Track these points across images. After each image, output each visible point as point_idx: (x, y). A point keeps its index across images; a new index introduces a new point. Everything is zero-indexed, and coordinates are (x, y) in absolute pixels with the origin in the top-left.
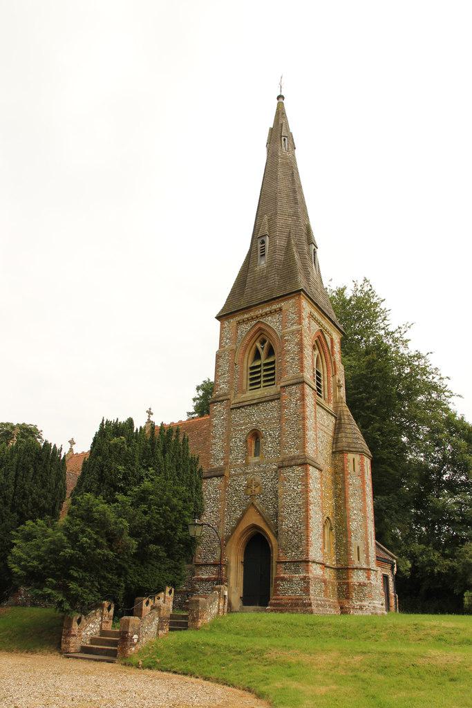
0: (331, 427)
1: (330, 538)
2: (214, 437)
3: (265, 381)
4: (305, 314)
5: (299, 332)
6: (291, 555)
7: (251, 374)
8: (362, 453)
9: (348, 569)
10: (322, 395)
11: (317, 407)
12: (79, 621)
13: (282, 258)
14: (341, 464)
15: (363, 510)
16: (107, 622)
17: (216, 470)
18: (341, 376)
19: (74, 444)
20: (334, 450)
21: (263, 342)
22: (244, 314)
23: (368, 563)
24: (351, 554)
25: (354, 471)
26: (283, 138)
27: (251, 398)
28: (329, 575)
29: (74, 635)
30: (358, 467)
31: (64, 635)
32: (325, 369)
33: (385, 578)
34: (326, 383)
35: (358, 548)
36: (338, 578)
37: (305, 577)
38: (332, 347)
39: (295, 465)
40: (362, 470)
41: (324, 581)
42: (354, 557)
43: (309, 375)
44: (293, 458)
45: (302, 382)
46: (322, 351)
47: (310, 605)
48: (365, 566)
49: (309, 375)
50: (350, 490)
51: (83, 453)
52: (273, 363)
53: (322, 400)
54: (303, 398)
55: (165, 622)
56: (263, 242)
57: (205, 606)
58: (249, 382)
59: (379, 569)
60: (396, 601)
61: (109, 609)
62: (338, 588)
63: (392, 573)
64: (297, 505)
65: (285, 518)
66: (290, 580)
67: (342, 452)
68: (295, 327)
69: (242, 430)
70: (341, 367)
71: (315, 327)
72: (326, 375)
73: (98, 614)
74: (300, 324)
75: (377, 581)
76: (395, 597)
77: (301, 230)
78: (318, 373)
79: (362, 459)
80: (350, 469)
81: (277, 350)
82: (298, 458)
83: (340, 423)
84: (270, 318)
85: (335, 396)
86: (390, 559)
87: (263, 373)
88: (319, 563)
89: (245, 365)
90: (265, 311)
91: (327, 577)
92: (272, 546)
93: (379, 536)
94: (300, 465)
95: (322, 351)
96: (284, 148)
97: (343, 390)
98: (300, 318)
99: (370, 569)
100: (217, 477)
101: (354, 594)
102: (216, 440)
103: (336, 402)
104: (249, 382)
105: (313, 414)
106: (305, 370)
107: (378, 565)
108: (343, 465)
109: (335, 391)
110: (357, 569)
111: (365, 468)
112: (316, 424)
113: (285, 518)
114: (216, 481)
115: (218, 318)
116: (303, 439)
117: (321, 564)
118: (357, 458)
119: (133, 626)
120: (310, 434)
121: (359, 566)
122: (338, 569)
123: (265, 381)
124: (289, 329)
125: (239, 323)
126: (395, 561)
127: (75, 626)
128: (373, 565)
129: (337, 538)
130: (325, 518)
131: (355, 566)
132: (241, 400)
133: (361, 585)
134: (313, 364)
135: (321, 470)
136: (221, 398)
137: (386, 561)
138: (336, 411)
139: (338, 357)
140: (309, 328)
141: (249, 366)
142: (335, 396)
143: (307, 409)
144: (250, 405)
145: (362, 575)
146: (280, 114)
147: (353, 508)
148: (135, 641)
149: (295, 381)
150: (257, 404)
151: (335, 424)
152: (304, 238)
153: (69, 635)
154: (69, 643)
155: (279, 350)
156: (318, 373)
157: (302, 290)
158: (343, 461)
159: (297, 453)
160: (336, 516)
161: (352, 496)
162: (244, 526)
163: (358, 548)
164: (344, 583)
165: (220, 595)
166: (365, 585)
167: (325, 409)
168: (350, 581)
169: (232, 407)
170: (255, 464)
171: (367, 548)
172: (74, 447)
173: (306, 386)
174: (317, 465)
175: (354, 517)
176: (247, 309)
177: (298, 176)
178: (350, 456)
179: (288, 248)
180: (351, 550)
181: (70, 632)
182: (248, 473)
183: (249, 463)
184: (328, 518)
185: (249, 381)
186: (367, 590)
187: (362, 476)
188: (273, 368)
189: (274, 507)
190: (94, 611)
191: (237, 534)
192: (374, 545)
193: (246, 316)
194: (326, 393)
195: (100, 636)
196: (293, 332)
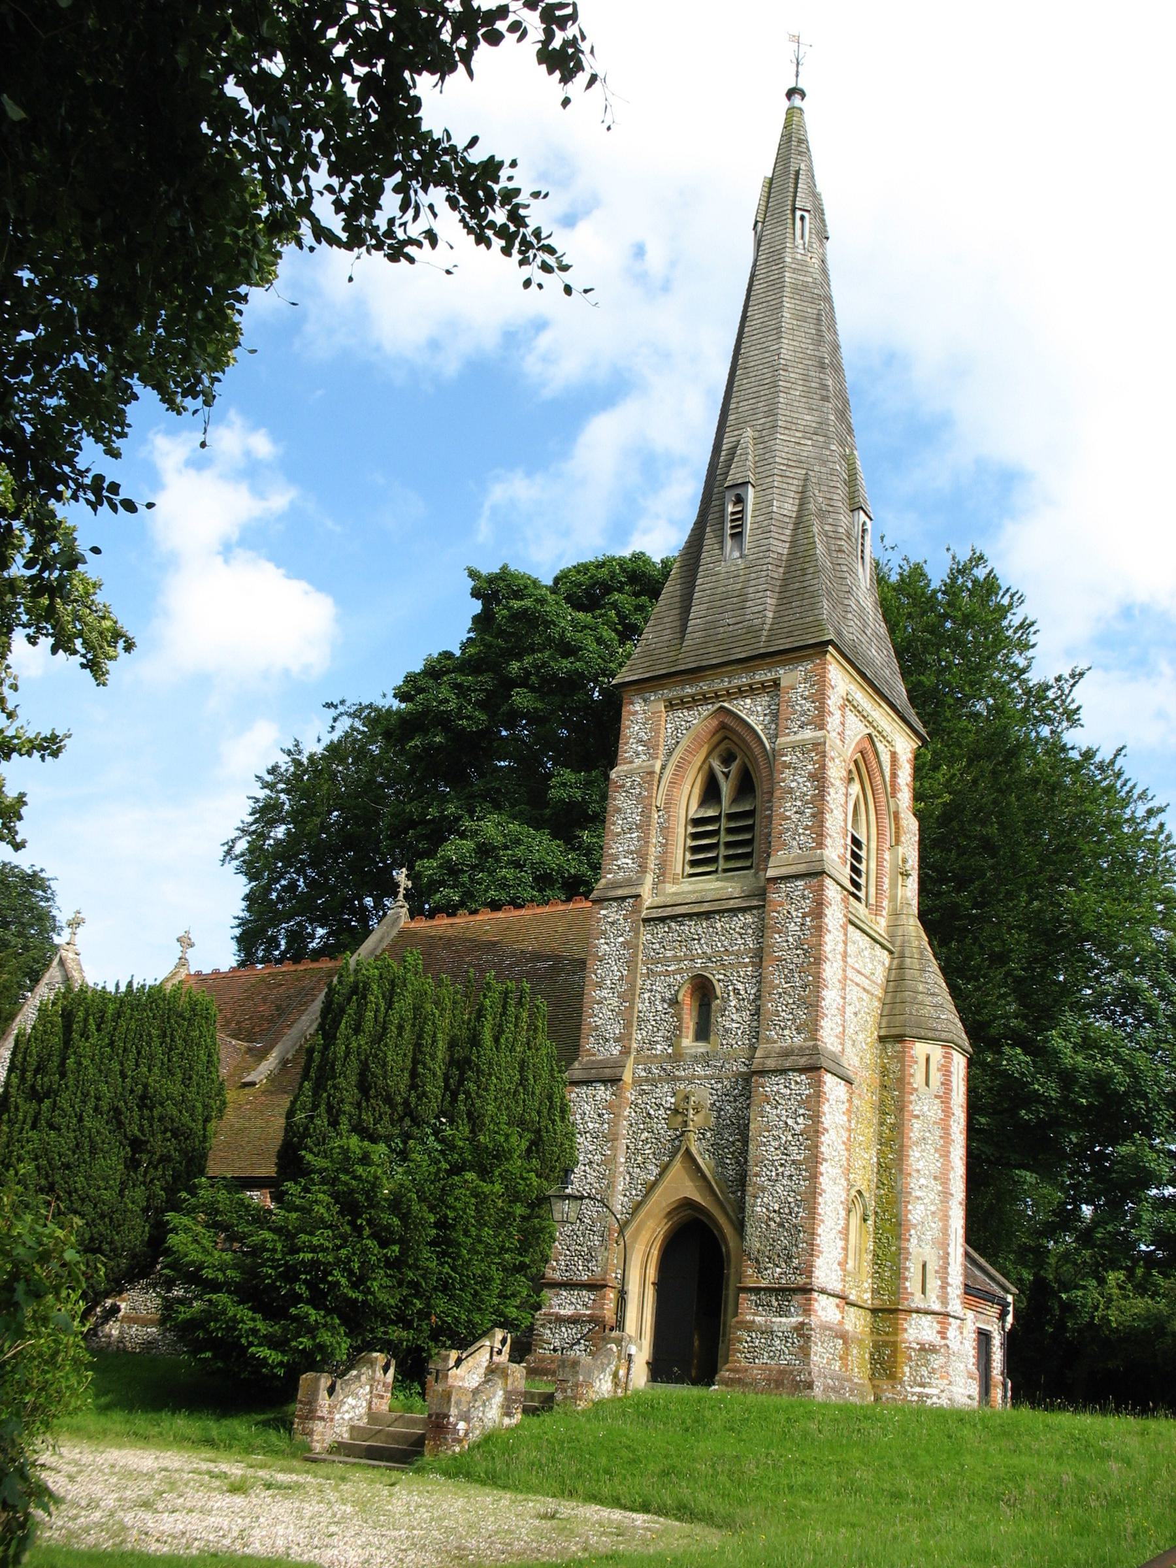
0: (880, 975)
1: (862, 1239)
2: (600, 986)
3: (728, 858)
4: (833, 702)
5: (818, 746)
6: (775, 1274)
7: (695, 836)
8: (948, 1043)
9: (897, 1310)
10: (862, 894)
11: (851, 928)
12: (331, 1390)
13: (784, 548)
14: (894, 1066)
15: (943, 1178)
16: (382, 1397)
17: (603, 1064)
18: (910, 850)
19: (192, 945)
20: (883, 1033)
21: (727, 760)
22: (683, 683)
23: (944, 1300)
24: (906, 1279)
25: (927, 1084)
26: (798, 213)
27: (693, 898)
28: (856, 1323)
29: (322, 1419)
30: (936, 1077)
31: (299, 1417)
32: (873, 830)
33: (984, 1337)
34: (873, 865)
35: (924, 1266)
36: (875, 1331)
37: (802, 1324)
38: (894, 775)
39: (794, 1070)
40: (946, 1084)
41: (843, 1336)
42: (912, 1285)
43: (835, 853)
44: (786, 1053)
45: (817, 874)
47: (810, 1386)
48: (937, 1307)
49: (835, 853)
50: (915, 1130)
51: (216, 972)
52: (750, 814)
53: (861, 908)
54: (818, 911)
55: (515, 1401)
56: (740, 500)
57: (589, 1373)
58: (689, 857)
59: (970, 1315)
60: (1005, 1396)
61: (386, 1369)
62: (872, 1354)
63: (1003, 1328)
64: (794, 1162)
65: (763, 1190)
66: (769, 1332)
67: (899, 1038)
68: (808, 734)
69: (667, 974)
70: (911, 824)
71: (856, 729)
72: (873, 845)
73: (363, 1378)
74: (821, 727)
75: (964, 1344)
76: (1004, 1385)
77: (833, 472)
78: (856, 842)
79: (947, 1057)
80: (918, 1080)
81: (761, 787)
82: (801, 1053)
83: (901, 967)
84: (748, 701)
85: (893, 898)
86: (1002, 1293)
87: (724, 838)
88: (833, 1296)
90: (736, 682)
91: (848, 1327)
92: (728, 1252)
93: (973, 1236)
94: (802, 1070)
96: (799, 241)
97: (913, 884)
98: (822, 711)
99: (947, 1315)
100: (604, 1082)
101: (907, 1369)
102: (604, 993)
103: (895, 914)
104: (689, 857)
105: (840, 948)
106: (828, 841)
107: (967, 1306)
108: (902, 1070)
109: (893, 885)
110: (918, 1311)
111: (954, 1079)
112: (844, 971)
113: (763, 1190)
114: (602, 1092)
116: (811, 1004)
117: (838, 1296)
118: (936, 1052)
119: (458, 1403)
120: (830, 997)
121: (922, 1306)
122: (874, 1311)
123: (728, 858)
124: (792, 738)
126: (1010, 1298)
127: (324, 1400)
128: (955, 1306)
129: (878, 1241)
130: (853, 1193)
131: (913, 1305)
132: (669, 901)
133: (926, 1350)
134: (845, 820)
135: (849, 1082)
136: (620, 892)
137: (989, 1297)
138: (892, 936)
139: (905, 798)
140: (841, 734)
141: (691, 815)
142: (893, 898)
143: (828, 938)
144: (690, 916)
145: (930, 1327)
146: (793, 114)
147: (918, 1171)
148: (461, 1433)
149: (802, 868)
150: (707, 915)
151: (890, 969)
152: (841, 492)
153: (311, 1415)
154: (310, 1433)
155: (766, 788)
156: (856, 842)
157: (830, 642)
158: (902, 1061)
159: (799, 1040)
160: (878, 1188)
161: (916, 1144)
163: (924, 1266)
164: (886, 1344)
165: (620, 1351)
166: (933, 1349)
167: (839, 884)
169: (644, 914)
170: (696, 1059)
171: (945, 1267)
172: (190, 954)
173: (828, 882)
174: (839, 1071)
175: (918, 1194)
176: (694, 673)
177: (833, 319)
178: (920, 1049)
179: (800, 522)
180: (907, 1269)
181: (312, 1411)
182: (679, 1079)
183: (681, 1055)
184: (859, 1192)
186: (937, 1361)
187: (945, 1099)
188: (750, 828)
189: (738, 1162)
190: (354, 1373)
192: (961, 1251)
193: (689, 690)
194: (872, 890)
195: (368, 1423)
196: (801, 747)
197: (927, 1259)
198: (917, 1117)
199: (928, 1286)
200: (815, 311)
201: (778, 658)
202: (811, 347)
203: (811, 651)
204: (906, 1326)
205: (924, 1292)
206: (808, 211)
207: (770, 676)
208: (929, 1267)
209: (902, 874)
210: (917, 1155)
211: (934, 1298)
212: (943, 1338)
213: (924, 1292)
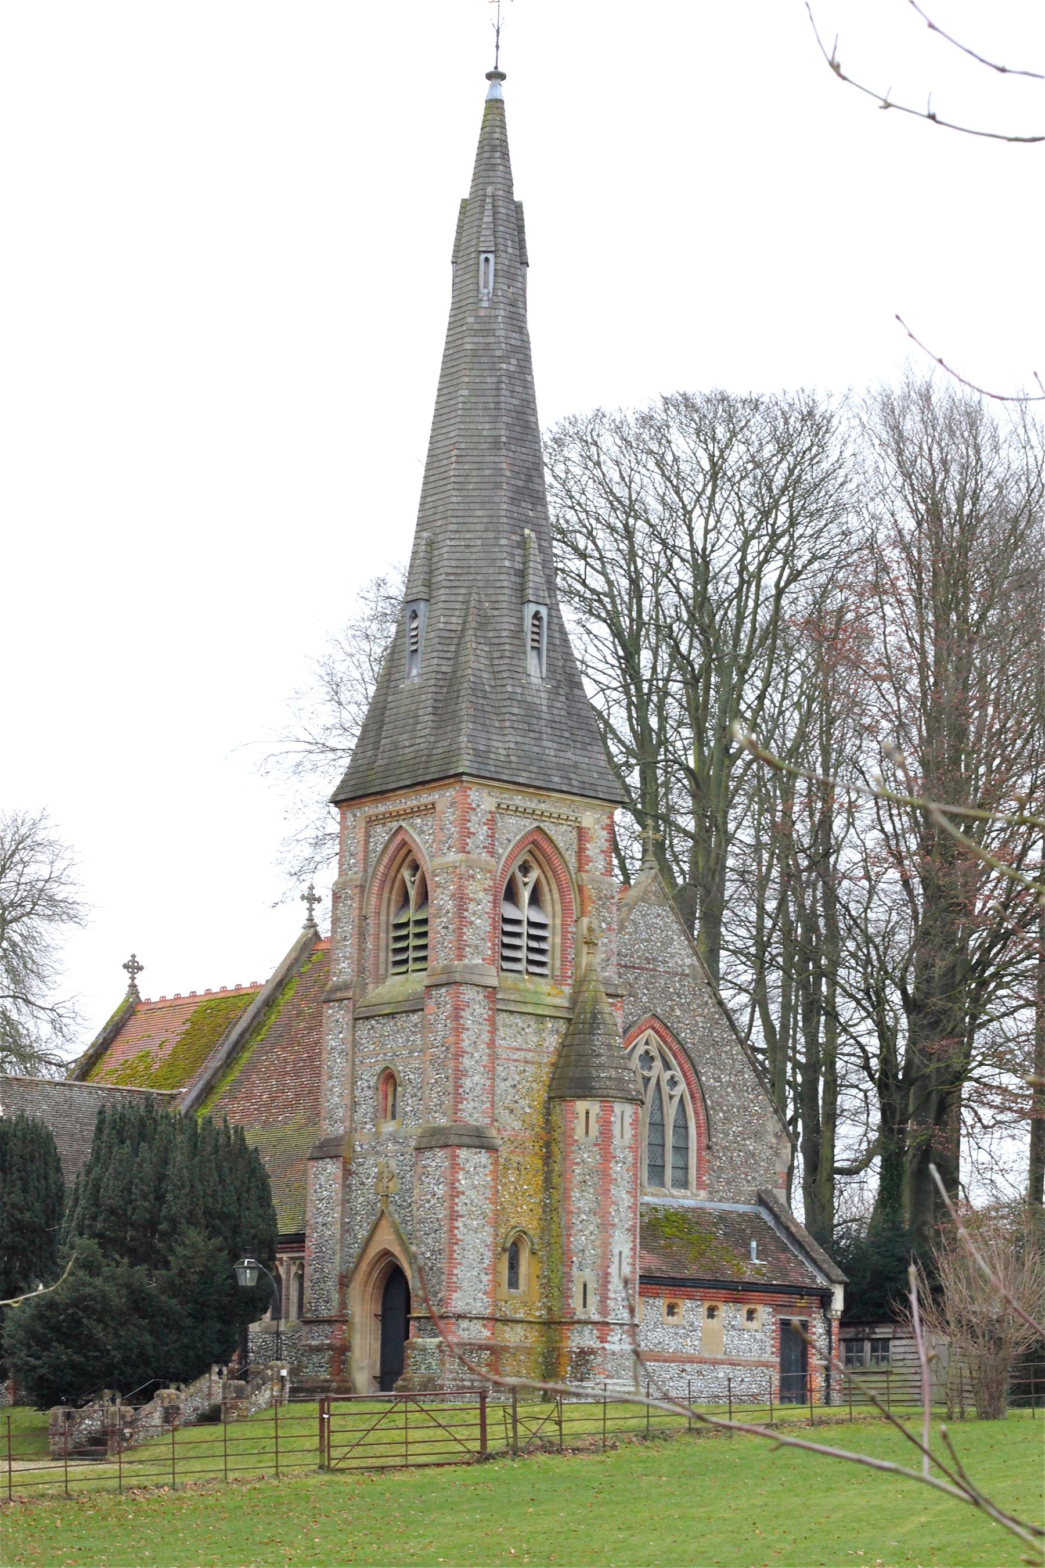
19: (140, 968)
23: (604, 1310)
30: (594, 1128)
35: (585, 1286)
42: (576, 1303)
46: (546, 868)
48: (596, 1317)
80: (579, 1132)
84: (419, 821)
89: (383, 918)
95: (546, 868)
100: (331, 1158)
115: (337, 803)
121: (583, 1317)
125: (371, 822)
131: (576, 1318)
135: (492, 1149)
146: (495, 108)
150: (391, 1015)
162: (373, 1252)
163: (585, 1286)
166: (592, 1352)
168: (563, 1345)
172: (139, 976)
185: (390, 954)
191: (364, 1266)
197: (588, 1279)
198: (578, 1164)
199: (588, 1301)
200: (495, 379)
201: (432, 785)
202: (487, 426)
203: (452, 780)
204: (569, 1334)
205: (585, 1306)
206: (491, 252)
207: (430, 799)
208: (589, 1286)
209: (586, 943)
210: (578, 1195)
211: (594, 1311)
212: (601, 1342)
213: (585, 1306)
